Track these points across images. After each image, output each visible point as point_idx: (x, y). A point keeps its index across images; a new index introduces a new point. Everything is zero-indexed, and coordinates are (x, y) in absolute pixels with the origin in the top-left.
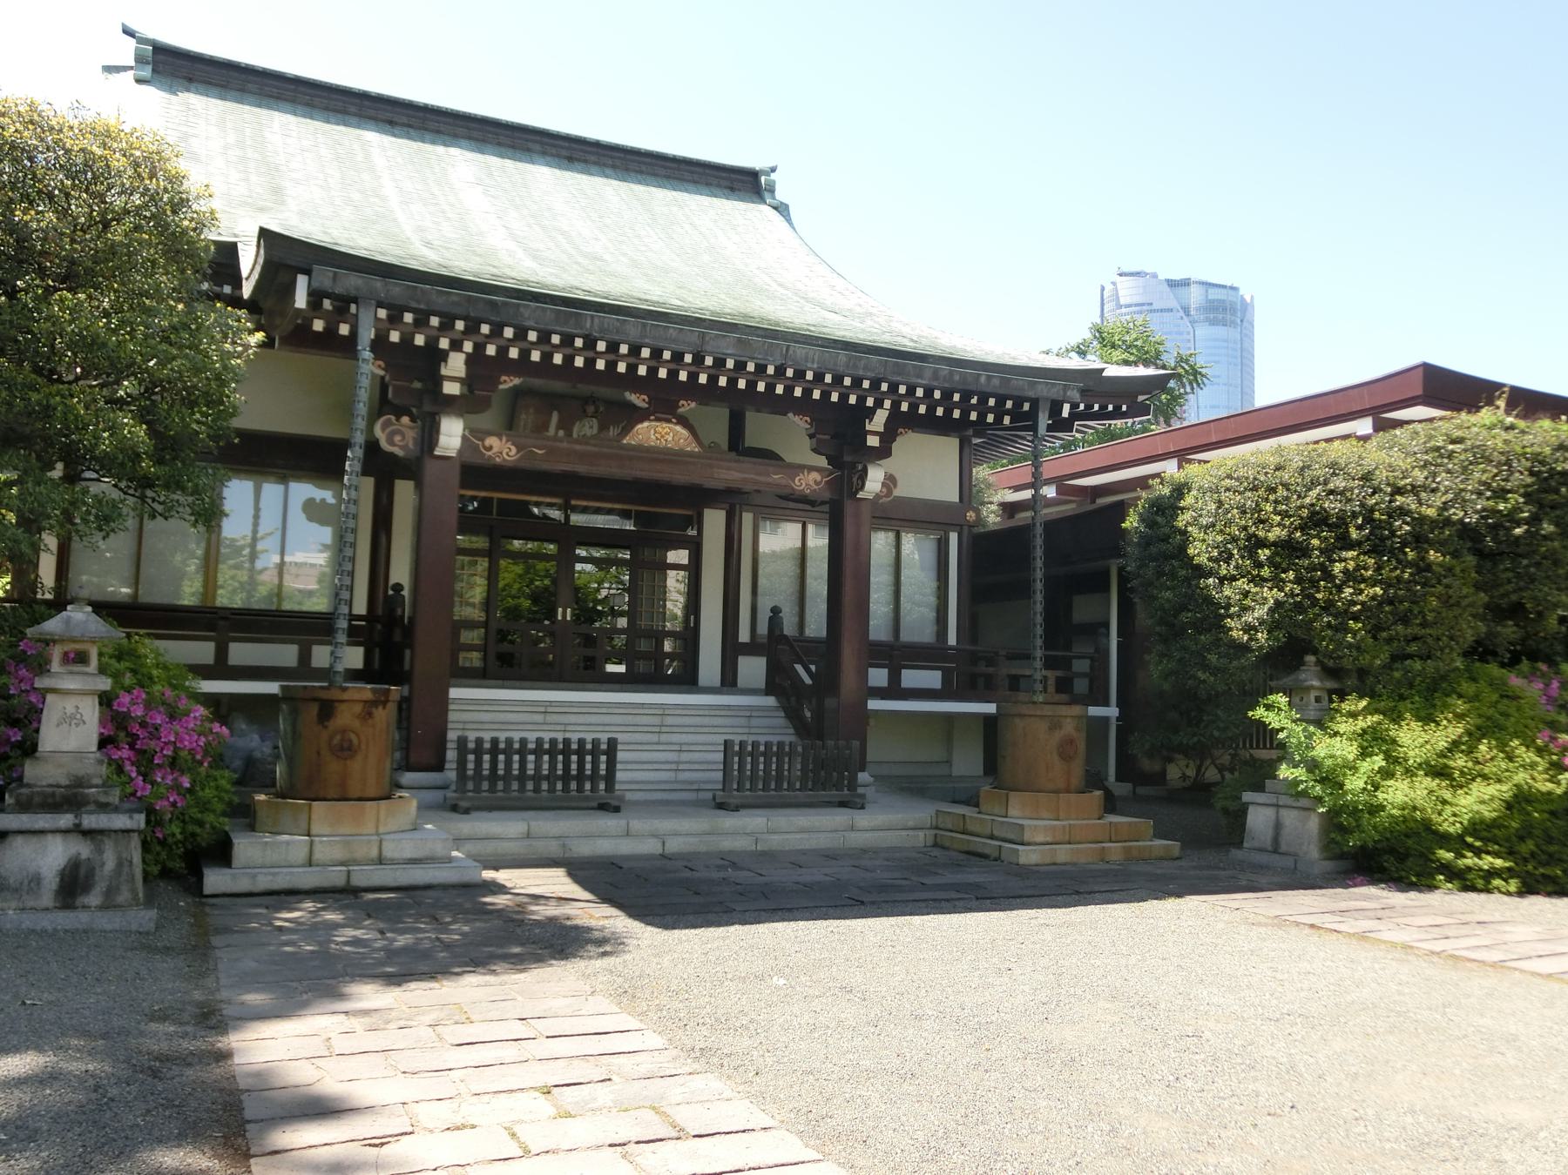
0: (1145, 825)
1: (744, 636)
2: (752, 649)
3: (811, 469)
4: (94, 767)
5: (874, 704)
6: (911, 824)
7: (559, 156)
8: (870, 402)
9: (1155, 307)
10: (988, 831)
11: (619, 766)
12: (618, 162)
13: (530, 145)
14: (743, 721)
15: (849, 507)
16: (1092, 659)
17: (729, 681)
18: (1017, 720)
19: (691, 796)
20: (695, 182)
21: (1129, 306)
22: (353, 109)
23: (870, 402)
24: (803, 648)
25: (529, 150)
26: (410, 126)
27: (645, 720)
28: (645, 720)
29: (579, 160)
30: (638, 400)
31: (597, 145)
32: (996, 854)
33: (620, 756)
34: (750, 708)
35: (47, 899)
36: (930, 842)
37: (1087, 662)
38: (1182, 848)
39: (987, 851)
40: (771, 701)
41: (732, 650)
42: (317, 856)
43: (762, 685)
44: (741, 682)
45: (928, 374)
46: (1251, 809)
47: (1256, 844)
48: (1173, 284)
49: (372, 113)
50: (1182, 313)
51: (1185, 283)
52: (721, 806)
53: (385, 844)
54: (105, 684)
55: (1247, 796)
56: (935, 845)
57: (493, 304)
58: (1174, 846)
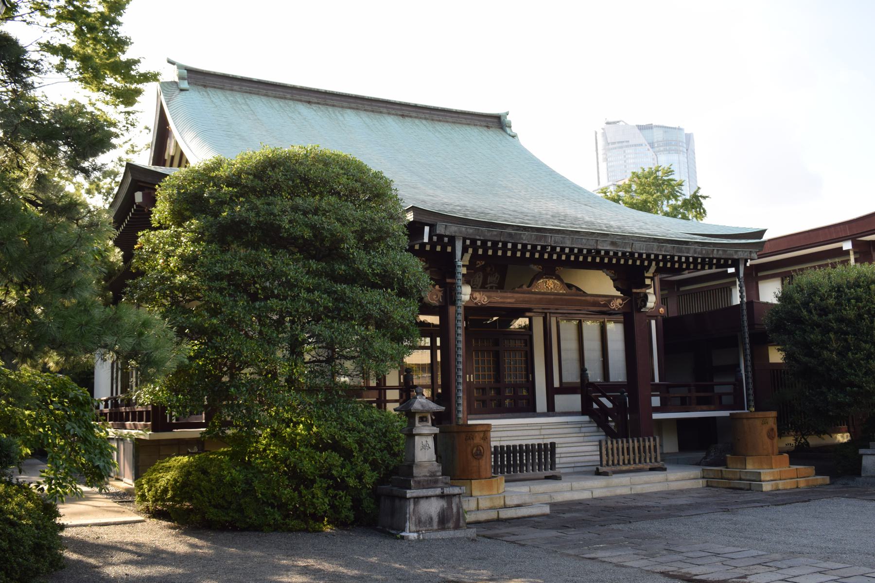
0: (811, 470)
1: (556, 384)
2: (566, 389)
3: (617, 297)
4: (437, 468)
5: (656, 416)
6: (692, 476)
7: (397, 115)
8: (646, 263)
9: (630, 143)
10: (738, 477)
11: (557, 456)
12: (427, 116)
13: (381, 109)
14: (577, 430)
15: (636, 317)
16: (734, 385)
17: (551, 410)
18: (745, 421)
19: (571, 470)
20: (469, 124)
21: (614, 143)
22: (289, 96)
23: (646, 263)
24: (606, 387)
25: (381, 112)
26: (319, 103)
27: (533, 432)
28: (533, 432)
29: (407, 116)
30: (536, 268)
31: (416, 106)
32: (748, 487)
33: (558, 450)
34: (578, 423)
35: (435, 526)
36: (705, 485)
37: (731, 387)
38: (831, 479)
39: (742, 486)
40: (586, 418)
41: (551, 393)
42: (481, 506)
43: (580, 410)
44: (557, 409)
45: (692, 251)
46: (864, 458)
47: (869, 474)
48: (641, 128)
49: (298, 97)
50: (648, 147)
51: (650, 127)
52: (598, 473)
53: (480, 501)
54: (436, 430)
55: (861, 451)
56: (708, 486)
57: (510, 234)
58: (827, 479)
